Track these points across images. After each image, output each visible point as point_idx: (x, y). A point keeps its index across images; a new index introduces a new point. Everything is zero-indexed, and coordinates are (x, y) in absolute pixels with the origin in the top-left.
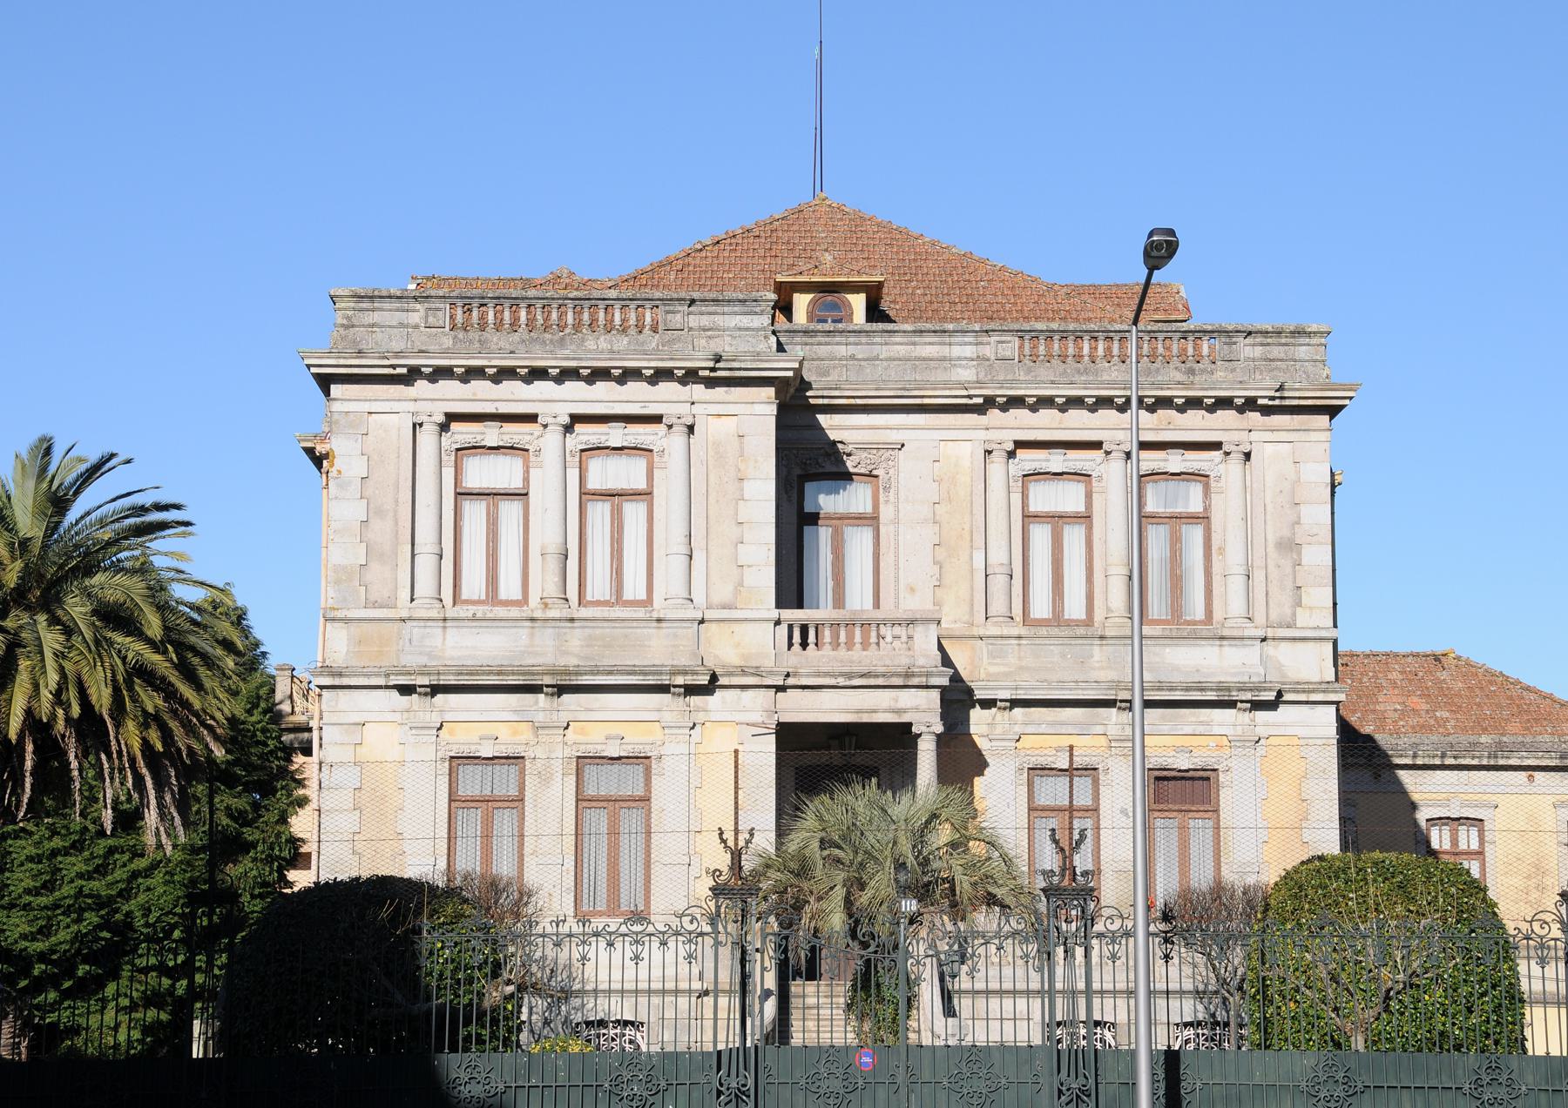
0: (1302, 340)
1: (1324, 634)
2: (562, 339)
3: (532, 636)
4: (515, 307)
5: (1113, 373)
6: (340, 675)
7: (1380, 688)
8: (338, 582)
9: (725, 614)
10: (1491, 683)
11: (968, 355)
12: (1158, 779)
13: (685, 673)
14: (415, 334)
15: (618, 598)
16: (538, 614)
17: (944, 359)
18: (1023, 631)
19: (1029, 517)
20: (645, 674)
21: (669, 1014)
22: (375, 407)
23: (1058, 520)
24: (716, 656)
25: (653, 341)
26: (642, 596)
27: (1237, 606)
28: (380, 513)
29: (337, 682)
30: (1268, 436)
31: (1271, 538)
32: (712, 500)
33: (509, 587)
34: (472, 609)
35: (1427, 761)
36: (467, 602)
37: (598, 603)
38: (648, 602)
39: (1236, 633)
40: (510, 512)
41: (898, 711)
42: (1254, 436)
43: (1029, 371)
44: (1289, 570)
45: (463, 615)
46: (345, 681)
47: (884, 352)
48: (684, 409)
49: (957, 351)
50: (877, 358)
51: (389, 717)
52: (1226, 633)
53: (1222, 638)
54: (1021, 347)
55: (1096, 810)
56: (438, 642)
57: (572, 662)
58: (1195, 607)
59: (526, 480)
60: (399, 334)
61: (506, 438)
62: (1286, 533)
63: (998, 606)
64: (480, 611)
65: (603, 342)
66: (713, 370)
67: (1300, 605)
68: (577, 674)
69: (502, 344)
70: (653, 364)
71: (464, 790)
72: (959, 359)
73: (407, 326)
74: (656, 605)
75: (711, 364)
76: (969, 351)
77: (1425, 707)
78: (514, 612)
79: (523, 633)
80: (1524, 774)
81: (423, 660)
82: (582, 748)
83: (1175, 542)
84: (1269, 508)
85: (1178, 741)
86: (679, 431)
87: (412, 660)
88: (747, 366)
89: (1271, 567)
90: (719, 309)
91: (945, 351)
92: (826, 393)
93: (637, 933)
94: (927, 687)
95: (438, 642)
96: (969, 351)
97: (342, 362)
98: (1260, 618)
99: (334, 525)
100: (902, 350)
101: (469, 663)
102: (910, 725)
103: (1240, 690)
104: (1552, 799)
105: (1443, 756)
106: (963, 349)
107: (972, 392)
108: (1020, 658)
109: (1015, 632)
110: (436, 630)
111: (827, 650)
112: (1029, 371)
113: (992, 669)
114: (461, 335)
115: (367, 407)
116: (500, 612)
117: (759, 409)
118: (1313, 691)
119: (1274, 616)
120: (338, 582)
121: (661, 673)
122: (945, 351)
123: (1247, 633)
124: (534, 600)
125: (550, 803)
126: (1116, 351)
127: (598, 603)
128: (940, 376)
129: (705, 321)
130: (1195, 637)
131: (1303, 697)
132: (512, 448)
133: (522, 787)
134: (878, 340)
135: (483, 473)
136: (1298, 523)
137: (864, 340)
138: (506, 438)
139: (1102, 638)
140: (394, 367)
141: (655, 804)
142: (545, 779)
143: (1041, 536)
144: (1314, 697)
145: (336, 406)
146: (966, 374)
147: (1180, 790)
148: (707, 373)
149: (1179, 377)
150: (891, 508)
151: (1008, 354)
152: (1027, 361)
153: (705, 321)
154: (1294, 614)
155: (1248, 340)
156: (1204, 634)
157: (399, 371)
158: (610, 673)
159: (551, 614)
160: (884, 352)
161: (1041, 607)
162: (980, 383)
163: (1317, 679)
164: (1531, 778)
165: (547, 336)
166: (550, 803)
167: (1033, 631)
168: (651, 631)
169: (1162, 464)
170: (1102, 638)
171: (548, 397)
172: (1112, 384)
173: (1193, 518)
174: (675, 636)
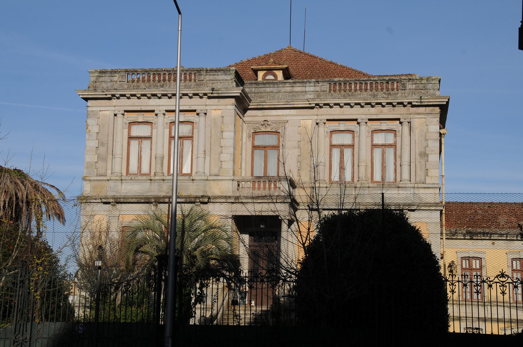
8: (88, 168)
9: (215, 178)
11: (312, 90)
16: (152, 178)
17: (303, 92)
19: (332, 146)
22: (102, 109)
23: (342, 147)
27: (406, 176)
28: (103, 144)
30: (417, 116)
31: (417, 151)
32: (212, 139)
35: (511, 238)
36: (130, 174)
39: (403, 186)
40: (146, 144)
42: (412, 116)
44: (424, 163)
48: (203, 108)
49: (308, 89)
52: (400, 185)
53: (398, 187)
54: (330, 87)
59: (152, 133)
60: (106, 84)
61: (145, 119)
62: (423, 150)
66: (212, 93)
67: (428, 176)
70: (192, 92)
72: (309, 92)
74: (193, 175)
75: (211, 92)
76: (312, 89)
84: (417, 141)
86: (202, 115)
87: (110, 194)
89: (417, 163)
90: (216, 73)
91: (303, 89)
92: (261, 104)
93: (503, 282)
96: (312, 89)
97: (90, 93)
98: (413, 180)
99: (87, 149)
101: (129, 194)
107: (311, 102)
115: (99, 109)
119: (418, 179)
120: (88, 168)
122: (303, 89)
123: (407, 186)
124: (152, 174)
126: (363, 87)
129: (212, 77)
132: (147, 122)
135: (138, 131)
136: (427, 146)
137: (276, 86)
138: (145, 119)
140: (106, 95)
143: (336, 152)
145: (89, 109)
151: (325, 89)
152: (332, 92)
154: (425, 179)
155: (410, 83)
160: (283, 90)
165: (159, 84)
168: (190, 183)
169: (379, 127)
171: (158, 104)
173: (390, 146)
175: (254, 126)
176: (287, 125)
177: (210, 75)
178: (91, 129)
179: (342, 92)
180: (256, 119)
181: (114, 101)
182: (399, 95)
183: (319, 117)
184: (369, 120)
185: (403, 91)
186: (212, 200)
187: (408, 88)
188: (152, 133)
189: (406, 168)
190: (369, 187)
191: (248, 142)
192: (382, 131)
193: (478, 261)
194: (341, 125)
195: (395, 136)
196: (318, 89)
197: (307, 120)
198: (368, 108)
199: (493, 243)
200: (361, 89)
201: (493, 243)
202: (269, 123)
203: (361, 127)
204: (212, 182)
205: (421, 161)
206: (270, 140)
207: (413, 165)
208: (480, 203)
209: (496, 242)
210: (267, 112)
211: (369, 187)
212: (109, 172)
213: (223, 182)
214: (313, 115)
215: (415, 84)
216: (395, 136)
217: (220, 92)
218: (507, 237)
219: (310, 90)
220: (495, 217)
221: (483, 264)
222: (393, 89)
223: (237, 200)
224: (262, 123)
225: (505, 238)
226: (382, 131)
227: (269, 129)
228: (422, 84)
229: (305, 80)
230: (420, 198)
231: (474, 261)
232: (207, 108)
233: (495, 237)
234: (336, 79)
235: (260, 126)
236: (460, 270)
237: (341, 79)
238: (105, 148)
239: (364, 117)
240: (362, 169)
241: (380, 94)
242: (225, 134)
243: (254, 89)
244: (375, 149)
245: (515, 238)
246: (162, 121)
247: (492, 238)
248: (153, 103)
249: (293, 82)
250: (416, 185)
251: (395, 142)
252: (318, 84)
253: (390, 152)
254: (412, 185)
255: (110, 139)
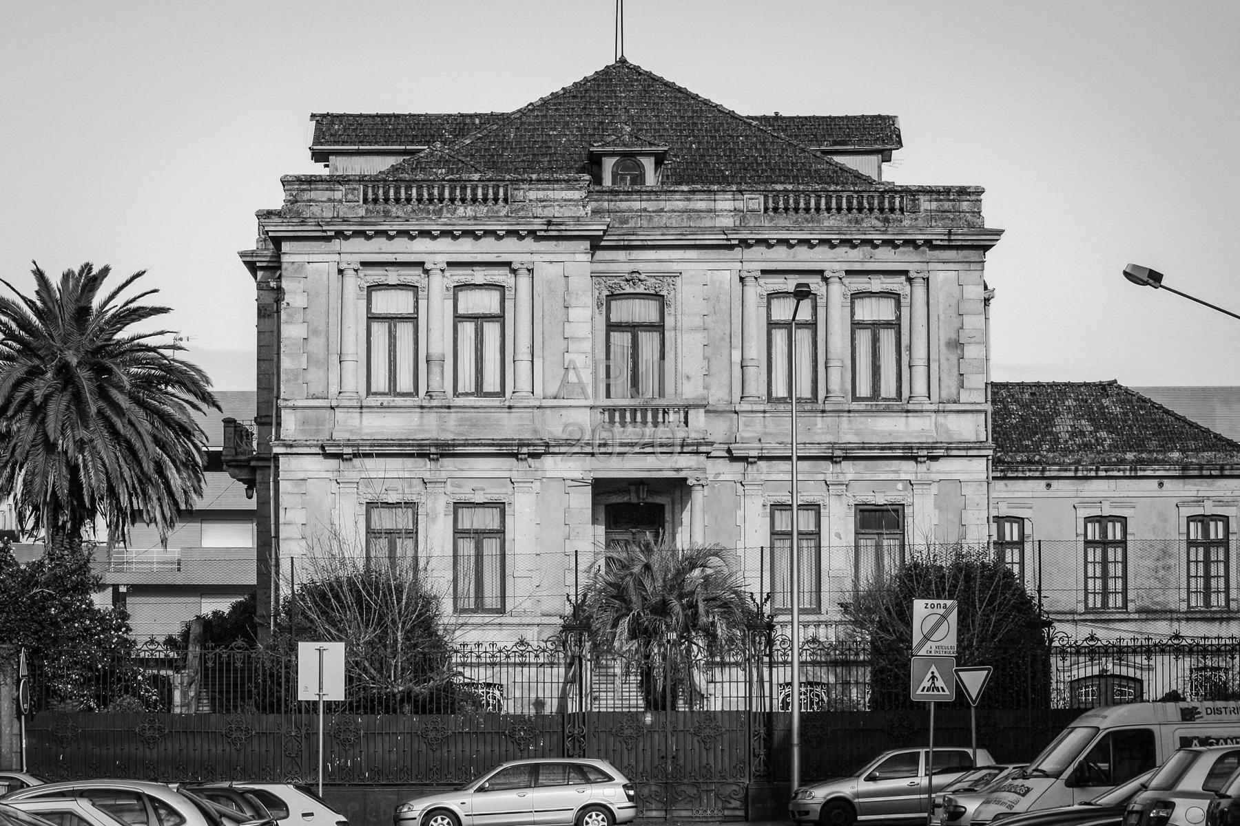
0: (964, 197)
1: (978, 407)
2: (441, 209)
3: (422, 417)
4: (408, 188)
5: (830, 221)
6: (291, 446)
7: (1058, 414)
10: (1141, 408)
11: (728, 208)
12: (861, 511)
13: (528, 445)
14: (339, 206)
15: (479, 391)
17: (710, 211)
18: (767, 408)
20: (500, 445)
21: (518, 679)
24: (550, 432)
25: (503, 210)
26: (498, 389)
28: (316, 332)
29: (289, 450)
30: (941, 266)
33: (404, 383)
34: (380, 399)
36: (375, 394)
37: (466, 394)
38: (502, 393)
41: (678, 470)
42: (932, 266)
43: (772, 219)
44: (955, 362)
45: (373, 404)
46: (294, 450)
47: (668, 206)
48: (526, 258)
50: (662, 210)
51: (324, 475)
52: (910, 407)
54: (766, 202)
55: (819, 534)
56: (356, 422)
57: (449, 436)
58: (888, 387)
59: (416, 307)
62: (954, 336)
63: (751, 389)
64: (386, 400)
65: (470, 211)
68: (454, 445)
69: (400, 213)
70: (505, 228)
71: (376, 525)
73: (334, 201)
76: (729, 205)
77: (1090, 429)
78: (409, 401)
79: (415, 417)
80: (1156, 482)
81: (347, 436)
82: (458, 497)
83: (875, 341)
84: (942, 317)
85: (880, 484)
88: (571, 228)
89: (942, 361)
90: (550, 186)
91: (711, 205)
94: (697, 453)
95: (356, 422)
96: (729, 205)
97: (290, 228)
98: (935, 397)
100: (680, 205)
102: (685, 479)
103: (919, 448)
104: (1175, 501)
105: (1097, 470)
106: (725, 203)
108: (765, 427)
109: (761, 408)
110: (355, 414)
111: (630, 429)
112: (772, 219)
113: (745, 435)
114: (371, 207)
115: (306, 258)
116: (399, 401)
117: (579, 257)
118: (970, 448)
119: (944, 395)
121: (511, 445)
122: (711, 205)
123: (925, 408)
125: (436, 538)
127: (466, 394)
128: (707, 223)
129: (541, 195)
130: (888, 410)
131: (963, 453)
133: (416, 523)
134: (663, 197)
137: (653, 197)
138: (402, 278)
139: (823, 411)
141: (508, 536)
142: (432, 518)
144: (971, 453)
146: (727, 222)
147: (879, 520)
148: (542, 233)
149: (878, 224)
150: (673, 319)
153: (541, 195)
156: (895, 408)
157: (329, 234)
158: (477, 445)
159: (434, 403)
160: (668, 206)
161: (780, 390)
162: (735, 229)
163: (973, 439)
164: (1161, 485)
165: (431, 207)
166: (436, 538)
167: (774, 406)
168: (504, 415)
170: (823, 411)
172: (830, 230)
174: (521, 418)
175: (610, 283)
176: (678, 280)
177: (538, 189)
178: (290, 301)
179: (791, 213)
180: (614, 267)
181: (336, 244)
182: (906, 223)
183: (747, 266)
184: (849, 273)
185: (913, 216)
186: (552, 450)
187: (922, 209)
188: (416, 307)
189: (920, 373)
190: (849, 411)
191: (597, 316)
192: (871, 294)
193: (1015, 526)
194: (789, 281)
195: (898, 306)
196: (739, 205)
197: (720, 272)
198: (842, 251)
199: (1049, 486)
200: (829, 209)
201: (1049, 486)
202: (642, 277)
203: (831, 286)
204: (548, 411)
205: (951, 356)
206: (645, 311)
207: (934, 366)
208: (1014, 385)
209: (1055, 483)
210: (636, 254)
211: (849, 411)
212: (334, 389)
213: (572, 411)
214: (733, 260)
215: (936, 200)
216: (898, 306)
217: (563, 227)
218: (1076, 470)
219: (725, 209)
220: (1049, 420)
221: (1027, 531)
222: (892, 210)
223: (600, 449)
224: (628, 276)
225: (1072, 474)
226: (871, 294)
227: (641, 290)
228: (949, 200)
229: (715, 188)
230: (948, 431)
231: (1007, 525)
232: (535, 258)
233: (1053, 471)
234: (779, 187)
235: (623, 283)
236: (820, 422)
237: (790, 187)
238: (321, 341)
239: (837, 266)
240: (835, 374)
241: (873, 221)
242: (573, 313)
243: (606, 204)
244: (858, 331)
245: (1093, 474)
246: (438, 284)
247: (1047, 474)
248: (419, 248)
249: (689, 192)
250: (941, 407)
251: (899, 318)
252: (740, 197)
253: (887, 337)
254: (934, 407)
255: (334, 320)
